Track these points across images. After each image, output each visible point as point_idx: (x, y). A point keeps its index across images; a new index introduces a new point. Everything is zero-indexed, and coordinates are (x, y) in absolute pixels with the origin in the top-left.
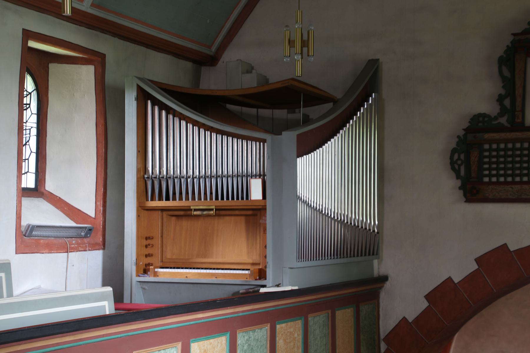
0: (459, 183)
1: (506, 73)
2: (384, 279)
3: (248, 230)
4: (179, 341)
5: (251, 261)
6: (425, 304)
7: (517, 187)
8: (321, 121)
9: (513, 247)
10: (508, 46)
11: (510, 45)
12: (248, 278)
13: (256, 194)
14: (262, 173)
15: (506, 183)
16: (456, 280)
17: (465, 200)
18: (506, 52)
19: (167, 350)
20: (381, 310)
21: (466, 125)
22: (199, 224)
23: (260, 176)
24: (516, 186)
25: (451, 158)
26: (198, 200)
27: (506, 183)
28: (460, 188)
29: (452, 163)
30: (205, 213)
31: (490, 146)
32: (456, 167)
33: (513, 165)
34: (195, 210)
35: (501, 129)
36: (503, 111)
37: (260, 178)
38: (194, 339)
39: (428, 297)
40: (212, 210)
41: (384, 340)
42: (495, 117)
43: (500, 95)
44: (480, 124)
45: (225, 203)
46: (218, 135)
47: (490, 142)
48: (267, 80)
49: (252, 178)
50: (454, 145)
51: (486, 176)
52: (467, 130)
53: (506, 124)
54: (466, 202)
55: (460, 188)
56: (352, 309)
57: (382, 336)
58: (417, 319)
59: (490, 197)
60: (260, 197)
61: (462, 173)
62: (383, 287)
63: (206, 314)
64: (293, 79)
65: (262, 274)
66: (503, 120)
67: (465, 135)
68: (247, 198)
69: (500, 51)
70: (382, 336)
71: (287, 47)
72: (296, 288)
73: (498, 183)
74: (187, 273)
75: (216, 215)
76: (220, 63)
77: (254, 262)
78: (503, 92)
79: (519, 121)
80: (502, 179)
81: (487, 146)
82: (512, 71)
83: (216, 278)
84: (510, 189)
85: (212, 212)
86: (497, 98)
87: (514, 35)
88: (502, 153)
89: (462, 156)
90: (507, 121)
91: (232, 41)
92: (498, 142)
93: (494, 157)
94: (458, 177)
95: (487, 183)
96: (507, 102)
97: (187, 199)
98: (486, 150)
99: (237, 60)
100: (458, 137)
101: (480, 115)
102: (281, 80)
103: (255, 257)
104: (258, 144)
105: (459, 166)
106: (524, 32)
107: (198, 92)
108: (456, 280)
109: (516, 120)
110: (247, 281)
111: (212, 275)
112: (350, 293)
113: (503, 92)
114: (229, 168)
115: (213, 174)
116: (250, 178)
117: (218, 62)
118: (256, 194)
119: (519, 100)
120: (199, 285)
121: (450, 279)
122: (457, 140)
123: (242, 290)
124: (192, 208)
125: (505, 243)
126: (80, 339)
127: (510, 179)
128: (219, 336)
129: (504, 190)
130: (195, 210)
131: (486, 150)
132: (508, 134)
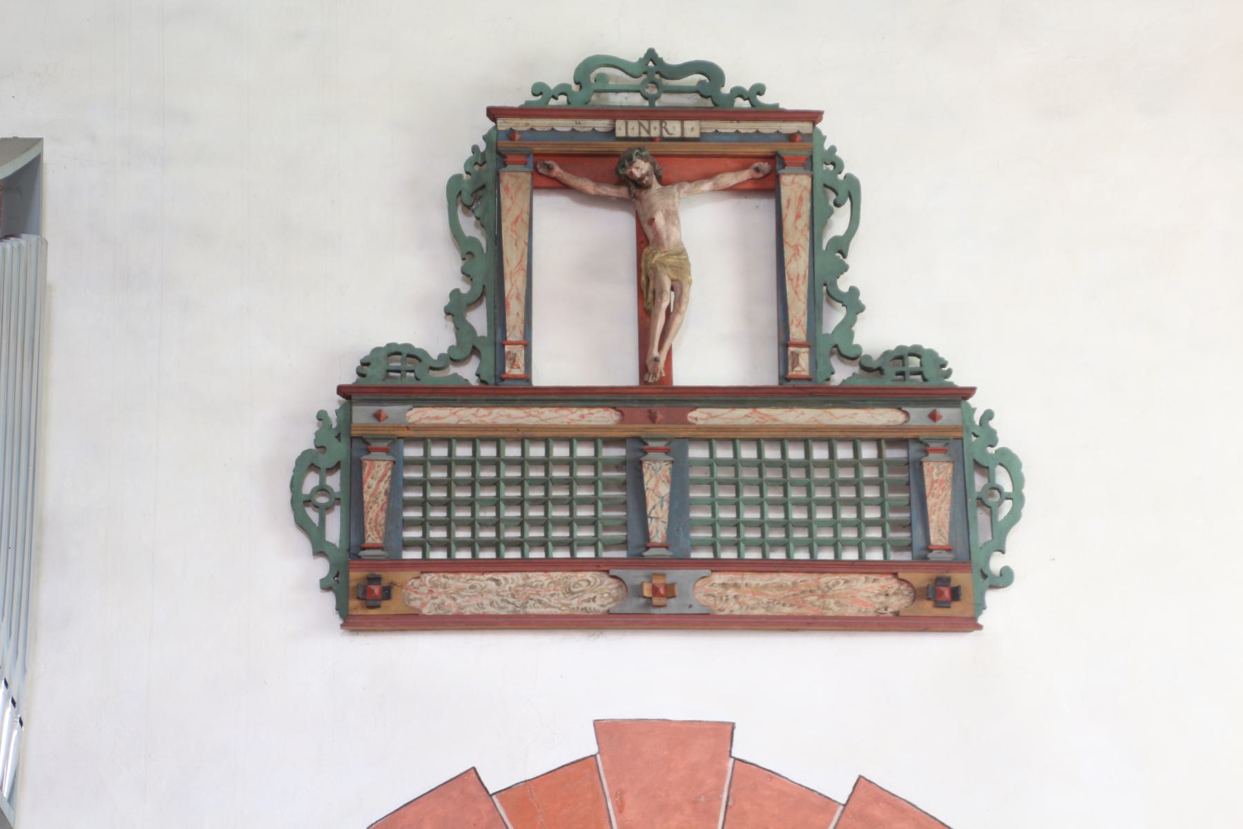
0: (321, 568)
1: (469, 226)
7: (515, 579)
9: (494, 782)
11: (483, 147)
18: (470, 163)
24: (509, 576)
25: (295, 485)
29: (300, 503)
31: (808, 453)
32: (313, 515)
50: (306, 442)
53: (474, 381)
55: (325, 586)
59: (425, 611)
61: (334, 530)
66: (468, 372)
67: (345, 414)
69: (455, 162)
81: (697, 452)
84: (492, 585)
86: (446, 300)
87: (493, 113)
93: (535, 482)
94: (320, 549)
95: (413, 564)
96: (478, 319)
101: (393, 351)
107: (548, 107)
109: (507, 370)
125: (472, 766)
129: (472, 587)
132: (482, 411)
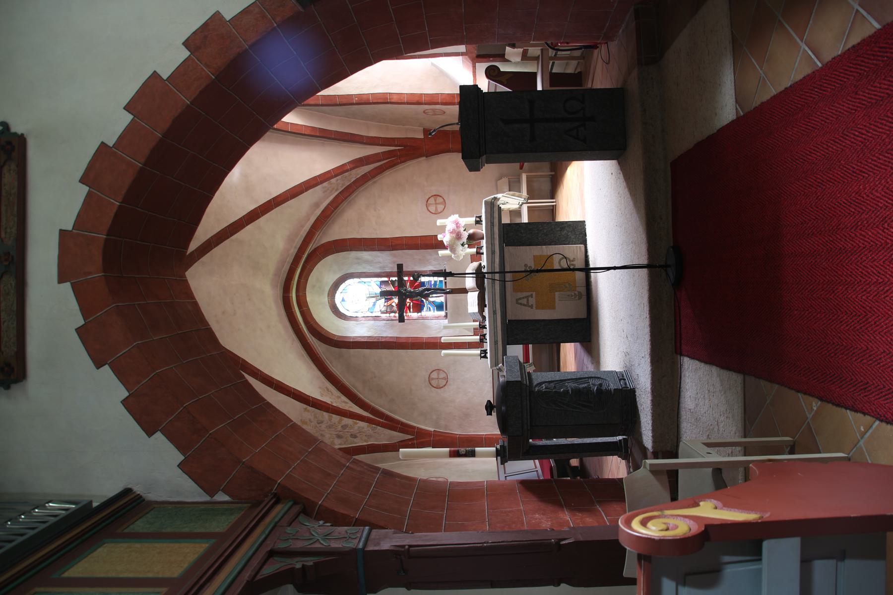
39: (150, 433)
41: (212, 496)
57: (206, 498)
58: (180, 448)
70: (206, 498)
84: (6, 324)
121: (124, 402)
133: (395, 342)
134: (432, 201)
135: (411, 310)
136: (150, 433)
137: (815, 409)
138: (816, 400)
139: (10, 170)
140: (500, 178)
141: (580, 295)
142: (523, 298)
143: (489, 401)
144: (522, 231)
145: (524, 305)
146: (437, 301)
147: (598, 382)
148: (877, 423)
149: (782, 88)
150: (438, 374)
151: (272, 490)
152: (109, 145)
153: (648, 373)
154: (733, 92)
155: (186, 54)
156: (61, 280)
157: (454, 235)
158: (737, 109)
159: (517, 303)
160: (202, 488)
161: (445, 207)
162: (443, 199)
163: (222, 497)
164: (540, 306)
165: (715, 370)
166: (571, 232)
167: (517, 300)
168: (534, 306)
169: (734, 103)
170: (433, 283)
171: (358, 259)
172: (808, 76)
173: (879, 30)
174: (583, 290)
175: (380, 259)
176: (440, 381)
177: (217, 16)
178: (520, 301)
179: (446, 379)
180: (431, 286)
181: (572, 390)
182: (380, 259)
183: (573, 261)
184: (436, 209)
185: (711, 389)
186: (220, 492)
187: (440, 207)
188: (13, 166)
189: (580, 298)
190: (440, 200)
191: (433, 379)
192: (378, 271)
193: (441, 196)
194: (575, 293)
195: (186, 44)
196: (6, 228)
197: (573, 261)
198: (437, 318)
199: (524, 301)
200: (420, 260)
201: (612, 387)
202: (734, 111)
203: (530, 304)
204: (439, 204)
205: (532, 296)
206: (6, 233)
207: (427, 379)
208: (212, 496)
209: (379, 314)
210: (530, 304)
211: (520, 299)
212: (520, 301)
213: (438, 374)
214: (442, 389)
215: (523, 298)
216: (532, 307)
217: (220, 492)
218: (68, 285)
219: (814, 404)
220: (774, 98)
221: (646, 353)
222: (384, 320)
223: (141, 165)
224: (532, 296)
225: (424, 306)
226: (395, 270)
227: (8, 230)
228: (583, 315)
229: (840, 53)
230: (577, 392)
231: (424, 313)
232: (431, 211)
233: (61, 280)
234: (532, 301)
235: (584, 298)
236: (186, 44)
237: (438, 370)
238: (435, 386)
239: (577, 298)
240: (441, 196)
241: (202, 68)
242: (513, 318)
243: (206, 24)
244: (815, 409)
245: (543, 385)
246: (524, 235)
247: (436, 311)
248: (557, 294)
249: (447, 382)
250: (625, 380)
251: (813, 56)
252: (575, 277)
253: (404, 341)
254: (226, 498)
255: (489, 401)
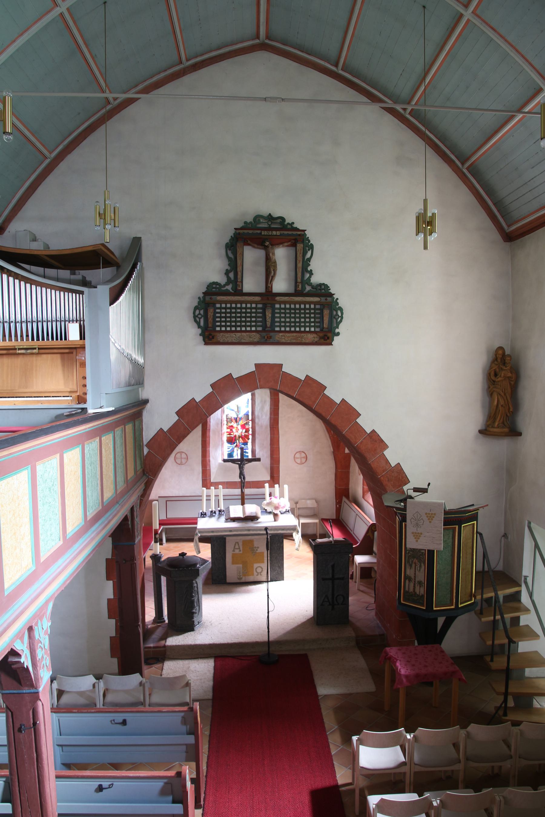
0: (199, 331)
1: (231, 255)
2: (146, 402)
3: (63, 365)
4: (57, 453)
5: (69, 390)
6: (176, 418)
7: (239, 334)
8: (118, 280)
10: (231, 236)
12: (70, 403)
13: (74, 333)
14: (78, 319)
15: (231, 331)
16: (198, 400)
17: (204, 343)
19: (52, 460)
20: (143, 424)
21: (204, 290)
22: (19, 361)
23: (77, 321)
24: (238, 334)
25: (194, 313)
26: (21, 341)
27: (231, 331)
28: (200, 335)
29: (195, 317)
30: (29, 351)
32: (198, 319)
33: (236, 319)
34: (19, 349)
35: (227, 293)
36: (229, 281)
37: (77, 322)
38: (65, 451)
39: (178, 413)
40: (35, 348)
41: (146, 445)
42: (224, 285)
43: (227, 270)
44: (213, 290)
45: (46, 343)
46: (38, 287)
47: (221, 302)
48: (49, 248)
49: (69, 322)
50: (196, 304)
51: (218, 326)
52: (205, 294)
54: (204, 344)
55: (200, 335)
56: (131, 424)
57: (145, 443)
58: (170, 429)
59: (221, 341)
60: (77, 338)
61: (202, 324)
62: (145, 408)
63: (73, 430)
64: (103, 245)
65: (82, 399)
66: (229, 288)
67: (204, 297)
68: (66, 339)
69: (227, 239)
70: (145, 443)
71: (98, 218)
72: (114, 409)
73: (226, 331)
74: (14, 401)
75: (38, 354)
76: (6, 232)
77: (72, 390)
78: (229, 268)
79: (240, 288)
80: (228, 329)
81: (218, 305)
82: (235, 253)
83: (42, 404)
84: (234, 335)
85: (35, 351)
87: (235, 229)
88: (228, 311)
89: (202, 312)
90: (232, 289)
91: (16, 215)
92: (226, 302)
94: (199, 327)
96: (231, 275)
97: (10, 339)
98: (218, 308)
99: (24, 230)
100: (199, 298)
101: (214, 283)
102: (80, 246)
103: (72, 386)
104: (74, 295)
105: (200, 318)
106: (242, 228)
108: (198, 400)
109: (238, 288)
110: (70, 405)
111: (38, 401)
112: (129, 414)
113: (229, 268)
114: (49, 313)
115: (23, 320)
116: (68, 323)
117: (5, 231)
118: (74, 333)
119: (239, 274)
120: (26, 410)
121: (193, 400)
122: (198, 300)
123: (66, 412)
124: (16, 347)
126: (11, 453)
127: (233, 329)
128: (76, 448)
129: (230, 336)
130: (19, 349)
131: (218, 308)
132: (233, 297)
133: (207, 429)
134: (303, 455)
135: (229, 436)
136: (178, 413)
137: (206, 733)
138: (209, 733)
139: (314, 338)
140: (317, 502)
141: (240, 579)
142: (239, 546)
143: (186, 554)
144: (278, 544)
145: (234, 547)
146: (234, 453)
147: (197, 611)
148: (207, 756)
149: (324, 718)
150: (184, 458)
151: (150, 476)
152: (325, 391)
153: (205, 642)
154: (329, 693)
155: (368, 431)
156: (257, 365)
157: (277, 505)
158: (322, 695)
159: (236, 543)
160: (150, 440)
161: (299, 464)
162: (304, 463)
163: (146, 450)
164: (234, 556)
165: (211, 683)
166: (278, 572)
167: (238, 543)
168: (234, 552)
169: (325, 694)
170: (247, 451)
171: (265, 402)
172: (325, 729)
173: (331, 754)
174: (243, 580)
175: (264, 417)
176: (180, 460)
177: (386, 447)
178: (237, 544)
179: (181, 464)
180: (245, 449)
181: (194, 600)
182: (264, 417)
183: (260, 574)
184: (298, 458)
185: (202, 681)
186: (148, 450)
187: (298, 461)
188: (316, 340)
189: (239, 579)
190: (304, 460)
191: (181, 455)
192: (256, 413)
193: (306, 461)
194: (241, 576)
195: (374, 431)
196: (284, 336)
197: (260, 574)
198: (223, 454)
199: (237, 547)
200: (263, 444)
201: (195, 619)
202: (321, 694)
203: (235, 550)
204: (301, 459)
205: (240, 551)
206: (282, 336)
207: (181, 451)
208: (146, 445)
209: (226, 413)
210: (235, 550)
211: (238, 544)
212: (237, 544)
213: (184, 458)
214: (174, 461)
215: (239, 546)
216: (234, 551)
217: (148, 450)
218: (254, 369)
219: (207, 732)
220: (321, 714)
221: (215, 641)
222: (222, 417)
223: (313, 408)
224: (240, 551)
225: (231, 444)
226: (257, 457)
227: (283, 337)
228: (229, 580)
229: (329, 741)
230: (193, 602)
231: (226, 445)
232: (296, 454)
233: (257, 365)
234: (237, 551)
235: (238, 581)
236: (374, 431)
237: (187, 458)
238: (176, 456)
239: (239, 577)
240: (306, 461)
241: (360, 440)
242: (227, 541)
243: (382, 441)
244: (206, 733)
245: (196, 585)
246: (276, 545)
247: (228, 453)
248: (241, 565)
249: (179, 464)
250: (198, 624)
251: (331, 731)
252: (250, 576)
253: (207, 435)
254: (145, 453)
255: (186, 554)
